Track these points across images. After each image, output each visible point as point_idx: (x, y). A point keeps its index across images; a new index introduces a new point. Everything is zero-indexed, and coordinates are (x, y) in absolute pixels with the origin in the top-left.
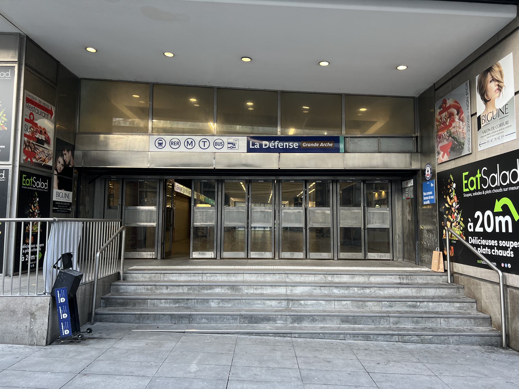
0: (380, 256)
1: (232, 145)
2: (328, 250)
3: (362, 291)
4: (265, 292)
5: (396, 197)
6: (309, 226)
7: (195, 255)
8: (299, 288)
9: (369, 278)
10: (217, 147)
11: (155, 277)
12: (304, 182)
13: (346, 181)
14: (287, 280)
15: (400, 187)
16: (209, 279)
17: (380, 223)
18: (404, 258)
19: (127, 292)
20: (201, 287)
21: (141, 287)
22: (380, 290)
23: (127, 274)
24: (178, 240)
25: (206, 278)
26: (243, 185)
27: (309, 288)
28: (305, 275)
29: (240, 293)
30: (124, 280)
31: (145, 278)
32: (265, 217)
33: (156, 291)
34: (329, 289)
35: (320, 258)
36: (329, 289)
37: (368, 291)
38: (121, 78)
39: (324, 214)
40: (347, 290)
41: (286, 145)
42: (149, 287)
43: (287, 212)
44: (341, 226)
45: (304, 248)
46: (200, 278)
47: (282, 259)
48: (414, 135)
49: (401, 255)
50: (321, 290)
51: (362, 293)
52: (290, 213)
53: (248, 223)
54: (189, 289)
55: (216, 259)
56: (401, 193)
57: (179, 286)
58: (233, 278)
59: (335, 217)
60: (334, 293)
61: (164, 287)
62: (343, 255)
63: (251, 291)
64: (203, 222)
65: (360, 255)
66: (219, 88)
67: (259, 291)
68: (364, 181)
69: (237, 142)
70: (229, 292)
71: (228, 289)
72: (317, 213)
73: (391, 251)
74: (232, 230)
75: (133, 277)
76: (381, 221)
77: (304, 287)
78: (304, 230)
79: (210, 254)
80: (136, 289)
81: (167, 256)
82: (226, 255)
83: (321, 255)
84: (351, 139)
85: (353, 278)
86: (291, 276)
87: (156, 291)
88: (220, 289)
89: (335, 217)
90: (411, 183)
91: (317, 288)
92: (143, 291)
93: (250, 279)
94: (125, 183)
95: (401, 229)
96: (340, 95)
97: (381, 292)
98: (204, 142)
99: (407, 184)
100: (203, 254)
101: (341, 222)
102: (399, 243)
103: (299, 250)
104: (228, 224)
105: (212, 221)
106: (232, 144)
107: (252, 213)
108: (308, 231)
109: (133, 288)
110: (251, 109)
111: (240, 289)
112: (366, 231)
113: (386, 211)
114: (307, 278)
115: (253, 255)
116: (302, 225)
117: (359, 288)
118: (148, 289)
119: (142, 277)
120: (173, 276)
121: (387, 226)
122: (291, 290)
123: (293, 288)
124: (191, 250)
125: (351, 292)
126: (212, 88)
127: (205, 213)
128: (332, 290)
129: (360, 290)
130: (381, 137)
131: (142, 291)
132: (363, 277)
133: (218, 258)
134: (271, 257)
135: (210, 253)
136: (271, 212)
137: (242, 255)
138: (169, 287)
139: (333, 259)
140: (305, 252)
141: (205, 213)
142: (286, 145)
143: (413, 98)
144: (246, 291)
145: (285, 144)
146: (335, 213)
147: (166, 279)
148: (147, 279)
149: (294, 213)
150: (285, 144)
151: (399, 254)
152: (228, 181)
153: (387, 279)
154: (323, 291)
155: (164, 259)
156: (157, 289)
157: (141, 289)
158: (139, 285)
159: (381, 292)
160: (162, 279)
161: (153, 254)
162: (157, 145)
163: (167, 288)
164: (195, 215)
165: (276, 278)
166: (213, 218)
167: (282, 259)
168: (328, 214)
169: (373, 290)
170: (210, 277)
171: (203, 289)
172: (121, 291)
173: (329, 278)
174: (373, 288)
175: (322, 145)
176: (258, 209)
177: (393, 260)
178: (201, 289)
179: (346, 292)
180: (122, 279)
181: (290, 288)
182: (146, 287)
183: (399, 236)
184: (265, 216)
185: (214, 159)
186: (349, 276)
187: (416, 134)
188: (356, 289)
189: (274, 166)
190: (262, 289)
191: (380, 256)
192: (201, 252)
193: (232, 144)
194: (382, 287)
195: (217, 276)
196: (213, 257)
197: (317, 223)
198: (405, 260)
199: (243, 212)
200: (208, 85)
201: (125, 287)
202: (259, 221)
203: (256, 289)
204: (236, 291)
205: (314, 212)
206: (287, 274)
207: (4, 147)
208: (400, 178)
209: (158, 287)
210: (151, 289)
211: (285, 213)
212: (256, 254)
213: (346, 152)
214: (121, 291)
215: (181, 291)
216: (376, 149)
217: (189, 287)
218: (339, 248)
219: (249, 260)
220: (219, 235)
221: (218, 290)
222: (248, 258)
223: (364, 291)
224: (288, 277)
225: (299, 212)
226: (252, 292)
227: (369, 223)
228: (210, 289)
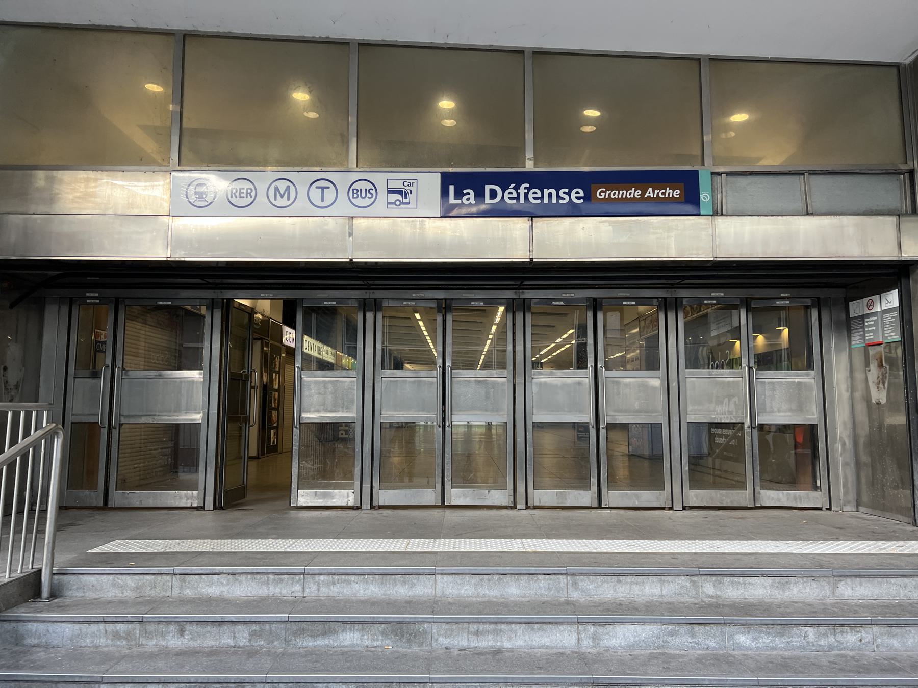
0: (795, 499)
1: (399, 197)
2: (656, 483)
3: (832, 639)
4: (507, 645)
5: (832, 341)
6: (605, 421)
7: (304, 497)
8: (620, 630)
9: (835, 587)
10: (359, 201)
11: (154, 586)
12: (724, 212)
13: (700, 300)
14: (575, 595)
15: (843, 316)
16: (324, 591)
17: (791, 410)
18: (858, 504)
19: (47, 647)
20: (295, 627)
21: (94, 627)
22: (890, 635)
23: (65, 578)
24: (256, 459)
25: (314, 588)
26: (428, 338)
27: (655, 628)
28: (629, 579)
29: (425, 648)
30: (53, 595)
31: (123, 588)
32: (487, 397)
33: (143, 641)
34: (723, 633)
35: (637, 504)
36: (723, 633)
37: (850, 638)
38: (97, 20)
39: (645, 387)
40: (781, 635)
41: (550, 195)
42: (121, 627)
43: (545, 383)
44: (691, 419)
45: (594, 480)
46: (298, 587)
47: (535, 508)
48: (903, 167)
49: (852, 496)
50: (693, 635)
51: (830, 648)
52: (555, 387)
53: (444, 412)
54: (253, 634)
55: (359, 508)
56: (845, 333)
57: (221, 623)
58: (401, 591)
59: (673, 396)
60: (739, 647)
61: (172, 628)
62: (696, 496)
63: (462, 640)
64: (326, 410)
65: (742, 497)
66: (364, 45)
67: (486, 642)
68: (746, 303)
69: (413, 189)
70: (388, 645)
71: (384, 633)
72: (627, 385)
73: (821, 482)
74: (406, 429)
75: (82, 588)
76: (794, 406)
77: (639, 628)
78: (593, 432)
79: (344, 497)
80: (80, 635)
81: (230, 498)
82: (386, 496)
83: (637, 496)
84: (730, 179)
85: (783, 586)
86: (587, 584)
87: (143, 641)
88: (357, 635)
89: (673, 396)
90: (892, 299)
91: (683, 629)
92: (102, 641)
93: (455, 592)
94: (121, 307)
95: (850, 425)
96: (696, 60)
97: (895, 643)
98: (323, 188)
99: (870, 305)
100: (324, 496)
101: (690, 408)
102: (846, 464)
103: (582, 483)
104: (391, 414)
105: (348, 409)
106: (399, 192)
107: (455, 385)
108: (603, 432)
109: (68, 630)
110: (449, 123)
111: (425, 632)
112: (755, 432)
113: (808, 379)
114: (636, 589)
115: (456, 496)
116: (587, 418)
117: (822, 630)
118: (116, 635)
119: (114, 585)
120: (211, 584)
121: (811, 415)
122: (595, 638)
123: (601, 630)
124: (294, 485)
125: (796, 641)
126: (343, 44)
127: (330, 386)
128: (731, 637)
129: (825, 635)
130: (813, 173)
131: (97, 642)
132: (814, 585)
133: (366, 505)
134: (505, 503)
135: (344, 492)
136: (503, 384)
137: (430, 496)
138: (188, 627)
139: (671, 508)
140: (595, 488)
141: (330, 388)
142: (550, 195)
143: (897, 66)
144: (444, 641)
145: (546, 192)
146: (674, 385)
147: (188, 592)
148: (128, 593)
149: (565, 385)
150: (546, 192)
151: (846, 493)
152: (392, 303)
153: (893, 590)
154: (700, 639)
155: (221, 508)
156: (147, 635)
157: (93, 635)
158: (89, 622)
159: (895, 643)
160: (176, 592)
161: (192, 497)
162: (193, 198)
163: (182, 632)
164: (306, 393)
165: (539, 589)
166: (352, 401)
167: (535, 508)
168: (654, 388)
169: (867, 634)
170: (328, 584)
171: (301, 632)
172: (29, 641)
173: (709, 588)
174: (868, 628)
175: (650, 193)
176: (466, 381)
177: (829, 509)
178: (295, 634)
179: (779, 642)
180: (45, 592)
181: (592, 629)
182: (110, 627)
183: (844, 444)
184: (487, 393)
185: (351, 235)
186: (769, 580)
187: (910, 163)
188: (811, 632)
189: (518, 254)
190: (496, 632)
191: (795, 499)
192: (320, 492)
193: (399, 192)
194: (898, 625)
195: (349, 582)
196: (351, 503)
197: (626, 411)
198: (861, 509)
199: (432, 383)
200: (335, 35)
201: (41, 626)
202: (472, 408)
203: (477, 633)
204: (409, 641)
205: (618, 383)
206: (573, 575)
207: (452, 188)
208: (841, 292)
209: (151, 628)
210: (128, 636)
211: (540, 384)
212: (465, 496)
213: (715, 213)
214: (29, 641)
215: (227, 641)
216: (799, 205)
217: (255, 627)
218: (686, 478)
219: (448, 512)
220: (366, 442)
221: (349, 639)
222: (443, 506)
223: (840, 637)
224: (575, 584)
225: (579, 383)
226: (464, 643)
227: (763, 410)
228: (324, 634)
